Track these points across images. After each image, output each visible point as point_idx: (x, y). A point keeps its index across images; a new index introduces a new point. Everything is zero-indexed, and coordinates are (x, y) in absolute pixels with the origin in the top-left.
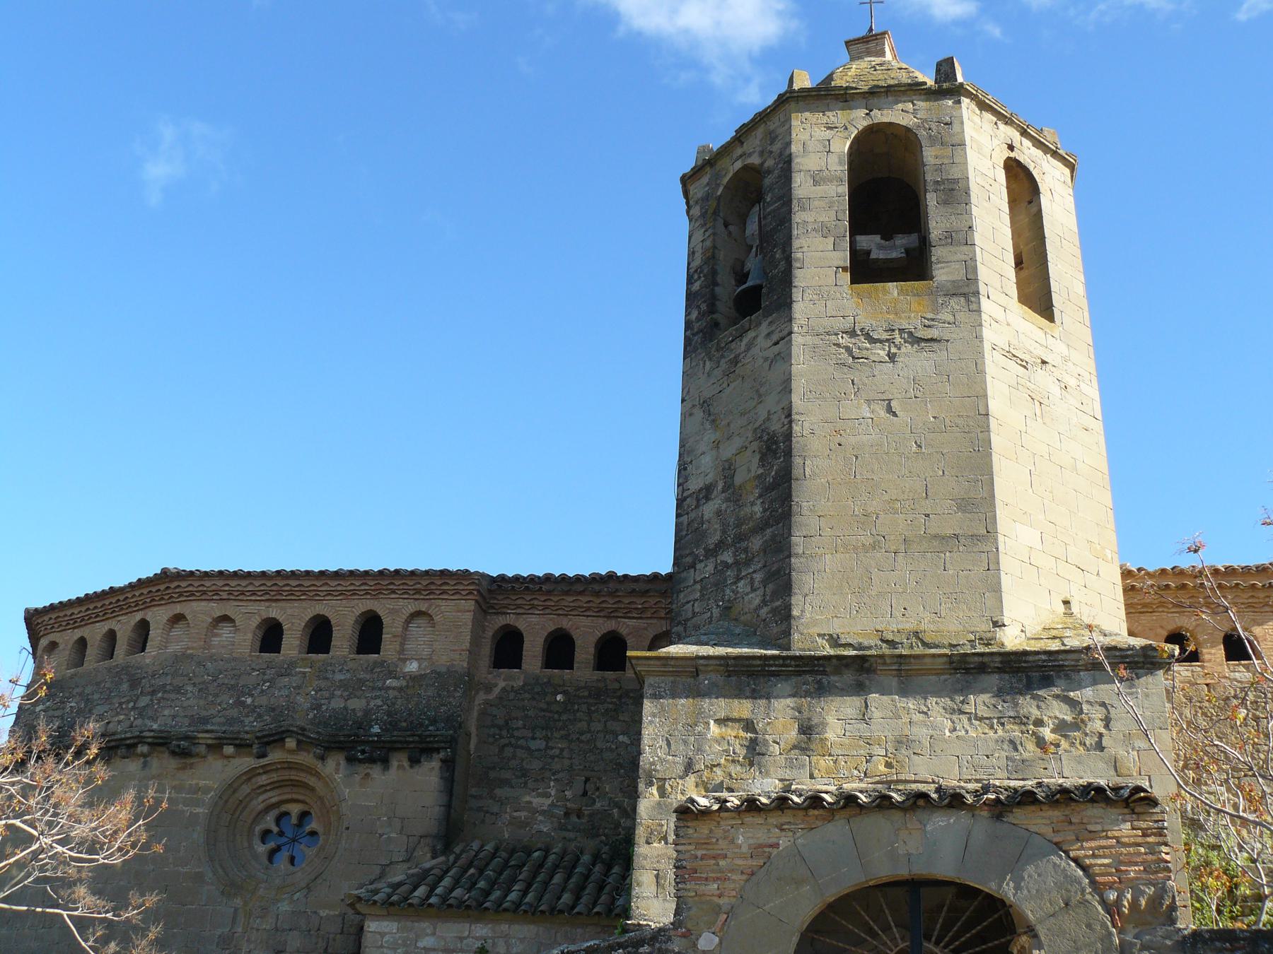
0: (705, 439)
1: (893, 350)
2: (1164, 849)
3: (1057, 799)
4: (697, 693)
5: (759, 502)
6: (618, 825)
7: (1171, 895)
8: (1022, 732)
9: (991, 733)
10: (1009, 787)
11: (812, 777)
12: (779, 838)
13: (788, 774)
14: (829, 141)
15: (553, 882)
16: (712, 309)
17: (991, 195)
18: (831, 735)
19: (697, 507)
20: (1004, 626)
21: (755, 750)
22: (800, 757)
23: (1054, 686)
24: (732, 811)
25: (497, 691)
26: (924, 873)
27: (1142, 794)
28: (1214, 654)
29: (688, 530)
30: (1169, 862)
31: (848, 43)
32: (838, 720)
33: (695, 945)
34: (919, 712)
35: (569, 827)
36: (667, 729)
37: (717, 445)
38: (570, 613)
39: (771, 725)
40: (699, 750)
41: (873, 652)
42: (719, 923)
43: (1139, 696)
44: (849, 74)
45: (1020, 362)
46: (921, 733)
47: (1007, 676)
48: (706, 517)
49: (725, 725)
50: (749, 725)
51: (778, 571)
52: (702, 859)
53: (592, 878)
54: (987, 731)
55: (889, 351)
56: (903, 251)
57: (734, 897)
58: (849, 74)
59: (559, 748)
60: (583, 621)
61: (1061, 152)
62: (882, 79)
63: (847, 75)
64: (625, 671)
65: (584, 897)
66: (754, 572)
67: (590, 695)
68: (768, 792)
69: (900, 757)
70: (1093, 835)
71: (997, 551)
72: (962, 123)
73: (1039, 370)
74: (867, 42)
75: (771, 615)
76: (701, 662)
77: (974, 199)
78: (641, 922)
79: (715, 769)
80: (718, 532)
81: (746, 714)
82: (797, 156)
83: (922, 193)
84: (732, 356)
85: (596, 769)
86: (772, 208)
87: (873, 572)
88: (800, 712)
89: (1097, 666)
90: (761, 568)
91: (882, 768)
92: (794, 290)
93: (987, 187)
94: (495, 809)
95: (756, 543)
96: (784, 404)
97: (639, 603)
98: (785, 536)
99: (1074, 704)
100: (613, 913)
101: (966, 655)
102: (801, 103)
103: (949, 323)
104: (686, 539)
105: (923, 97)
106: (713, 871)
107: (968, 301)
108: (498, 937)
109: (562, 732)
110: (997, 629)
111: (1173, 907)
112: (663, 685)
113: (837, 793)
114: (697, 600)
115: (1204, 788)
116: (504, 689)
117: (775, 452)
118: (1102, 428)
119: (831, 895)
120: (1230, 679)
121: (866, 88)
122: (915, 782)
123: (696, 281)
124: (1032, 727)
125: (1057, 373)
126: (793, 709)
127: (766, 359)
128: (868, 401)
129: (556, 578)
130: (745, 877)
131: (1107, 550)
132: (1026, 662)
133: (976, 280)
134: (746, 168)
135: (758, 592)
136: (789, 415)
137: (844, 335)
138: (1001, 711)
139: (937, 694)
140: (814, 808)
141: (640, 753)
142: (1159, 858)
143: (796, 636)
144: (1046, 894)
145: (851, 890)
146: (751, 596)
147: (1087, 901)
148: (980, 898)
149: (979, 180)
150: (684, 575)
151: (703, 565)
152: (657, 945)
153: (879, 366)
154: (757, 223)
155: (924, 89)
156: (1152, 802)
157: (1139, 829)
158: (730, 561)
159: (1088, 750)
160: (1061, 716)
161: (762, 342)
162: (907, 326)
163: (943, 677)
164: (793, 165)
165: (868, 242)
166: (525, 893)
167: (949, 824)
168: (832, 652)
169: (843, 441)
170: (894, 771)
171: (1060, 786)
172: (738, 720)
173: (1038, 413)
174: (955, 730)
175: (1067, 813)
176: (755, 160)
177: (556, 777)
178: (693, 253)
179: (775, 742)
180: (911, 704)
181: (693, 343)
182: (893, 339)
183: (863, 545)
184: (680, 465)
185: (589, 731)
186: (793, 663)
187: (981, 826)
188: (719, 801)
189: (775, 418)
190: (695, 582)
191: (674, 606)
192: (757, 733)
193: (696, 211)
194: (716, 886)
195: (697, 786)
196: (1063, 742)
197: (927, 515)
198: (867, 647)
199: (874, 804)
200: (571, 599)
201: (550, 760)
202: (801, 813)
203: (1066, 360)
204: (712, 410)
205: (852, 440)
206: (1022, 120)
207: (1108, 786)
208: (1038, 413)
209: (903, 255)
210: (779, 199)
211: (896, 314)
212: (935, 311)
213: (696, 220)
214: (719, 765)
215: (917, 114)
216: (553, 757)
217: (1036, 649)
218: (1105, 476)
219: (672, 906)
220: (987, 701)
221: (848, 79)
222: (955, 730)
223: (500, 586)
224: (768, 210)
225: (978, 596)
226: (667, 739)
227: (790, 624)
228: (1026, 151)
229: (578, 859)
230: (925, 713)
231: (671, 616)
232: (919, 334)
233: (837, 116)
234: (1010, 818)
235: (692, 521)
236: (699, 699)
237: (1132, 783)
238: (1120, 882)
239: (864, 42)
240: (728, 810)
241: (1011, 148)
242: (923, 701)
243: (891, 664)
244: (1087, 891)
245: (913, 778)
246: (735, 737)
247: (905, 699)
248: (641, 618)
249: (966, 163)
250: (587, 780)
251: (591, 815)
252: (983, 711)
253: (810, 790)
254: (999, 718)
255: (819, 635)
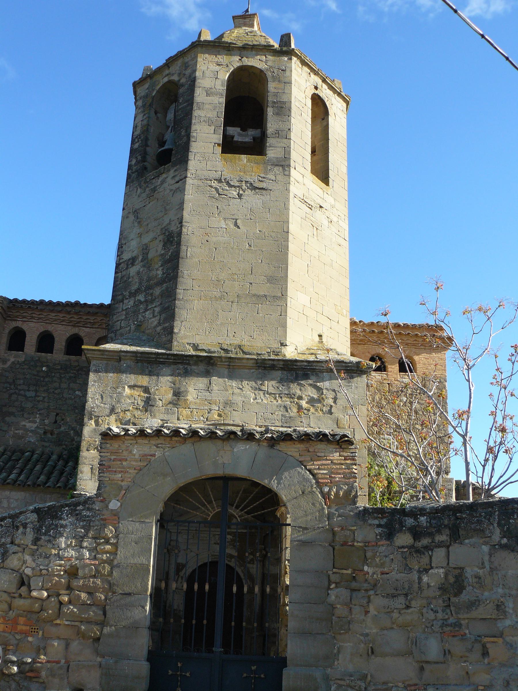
0: (134, 231)
1: (241, 192)
2: (354, 467)
3: (303, 439)
4: (119, 371)
5: (160, 269)
6: (73, 440)
7: (355, 490)
8: (291, 402)
9: (275, 402)
10: (279, 431)
11: (178, 419)
12: (156, 451)
13: (166, 417)
14: (217, 72)
15: (36, 469)
16: (144, 160)
17: (302, 113)
18: (190, 398)
19: (127, 268)
20: (286, 345)
21: (149, 403)
22: (172, 408)
23: (310, 379)
24: (131, 436)
25: (9, 363)
26: (231, 473)
27: (346, 439)
28: (394, 368)
29: (120, 281)
30: (356, 474)
31: (234, 18)
32: (194, 389)
33: (107, 506)
34: (238, 388)
35: (46, 440)
36: (101, 389)
37: (140, 235)
38: (53, 322)
39: (158, 391)
40: (119, 402)
41: (216, 355)
42: (121, 495)
43: (353, 388)
44: (233, 35)
45: (308, 205)
46: (238, 399)
47: (285, 372)
48: (131, 275)
49: (133, 389)
50: (146, 390)
51: (168, 307)
52: (113, 461)
53: (57, 468)
54: (273, 400)
55: (239, 193)
56: (252, 138)
57: (130, 481)
58: (233, 35)
59: (43, 396)
60: (60, 328)
61: (343, 94)
62: (250, 40)
63: (231, 36)
64: (81, 356)
65: (52, 478)
66: (155, 307)
67: (61, 368)
68: (152, 427)
69: (226, 411)
70: (319, 458)
71: (286, 306)
72: (291, 71)
73: (318, 211)
74: (245, 18)
75: (162, 331)
76: (123, 354)
77: (293, 114)
78: (82, 493)
79: (126, 412)
80: (137, 284)
81: (145, 384)
82: (199, 79)
83: (266, 107)
84: (153, 187)
85: (62, 409)
86: (182, 106)
87: (220, 312)
88: (174, 384)
89: (331, 370)
90: (159, 305)
91: (216, 417)
92: (190, 153)
93: (301, 108)
94: (5, 428)
95: (157, 291)
96: (179, 216)
97: (92, 319)
98: (173, 289)
99: (319, 389)
100: (68, 487)
101: (265, 360)
102: (204, 49)
103: (272, 181)
104: (120, 286)
105: (272, 54)
106: (119, 467)
107: (284, 169)
108: (4, 498)
109: (45, 388)
110: (283, 347)
111: (356, 496)
112: (101, 365)
113: (188, 429)
114: (123, 320)
115: (381, 436)
116: (13, 363)
117: (172, 242)
118: (348, 245)
119: (182, 482)
121: (241, 44)
122: (233, 425)
123: (136, 143)
124: (296, 400)
125: (327, 213)
126: (171, 382)
127: (171, 190)
128: (225, 219)
129: (46, 302)
130: (136, 471)
131: (344, 310)
132: (296, 365)
133: (290, 158)
134: (170, 82)
135: (157, 318)
136: (181, 222)
137: (215, 181)
138: (281, 391)
139: (249, 379)
140: (176, 437)
141: (86, 402)
142: (351, 471)
143: (175, 343)
144: (293, 487)
145: (192, 480)
146: (152, 320)
147: (313, 491)
148: (259, 488)
149: (297, 104)
150: (117, 306)
151: (127, 301)
152: (87, 506)
153: (232, 200)
154: (173, 114)
155: (272, 49)
156: (350, 443)
157: (343, 456)
158: (143, 300)
159: (324, 414)
160: (312, 395)
161: (170, 181)
162: (250, 180)
163: (252, 371)
164: (196, 83)
165: (233, 131)
166: (20, 474)
167: (246, 448)
168: (194, 353)
169: (209, 239)
170: (222, 418)
171: (305, 432)
172: (141, 387)
173: (315, 233)
174: (256, 399)
175: (308, 446)
176: (175, 78)
177: (40, 412)
178: (136, 127)
179: (160, 399)
180: (234, 384)
181: (132, 177)
182: (242, 186)
183: (215, 297)
184: (119, 245)
185: (60, 388)
186: (172, 358)
187: (263, 451)
188: (125, 430)
189: (173, 223)
190: (123, 310)
191: (110, 322)
192: (150, 394)
193: (140, 103)
194: (120, 475)
195: (116, 421)
196: (311, 409)
197: (251, 284)
198: (213, 352)
199: (207, 436)
200: (54, 314)
201: (37, 403)
202: (168, 439)
203: (333, 207)
204: (139, 216)
205: (214, 239)
206: (323, 73)
207: (330, 433)
208: (315, 233)
209: (252, 140)
210: (186, 101)
211: (245, 172)
212: (266, 173)
213: (139, 108)
214: (129, 410)
215: (267, 63)
216: (39, 401)
217: (302, 359)
218: (347, 271)
219: (97, 484)
220: (274, 385)
221: (232, 38)
222: (256, 399)
223: (14, 305)
224: (180, 107)
225: (274, 329)
226: (101, 395)
227: (172, 337)
228: (324, 91)
229: (50, 457)
230: (240, 389)
231: (109, 328)
232: (256, 185)
233: (223, 59)
234: (278, 447)
235: (124, 276)
236: (120, 374)
237: (340, 432)
238: (331, 483)
239: (243, 18)
240: (129, 435)
241: (316, 88)
242: (240, 383)
243: (225, 362)
244: (314, 487)
245: (232, 422)
246: (138, 396)
247: (231, 381)
248: (92, 328)
249: (291, 93)
250: (57, 414)
251: (57, 434)
252: (271, 390)
253: (174, 427)
254: (279, 394)
255: (188, 344)
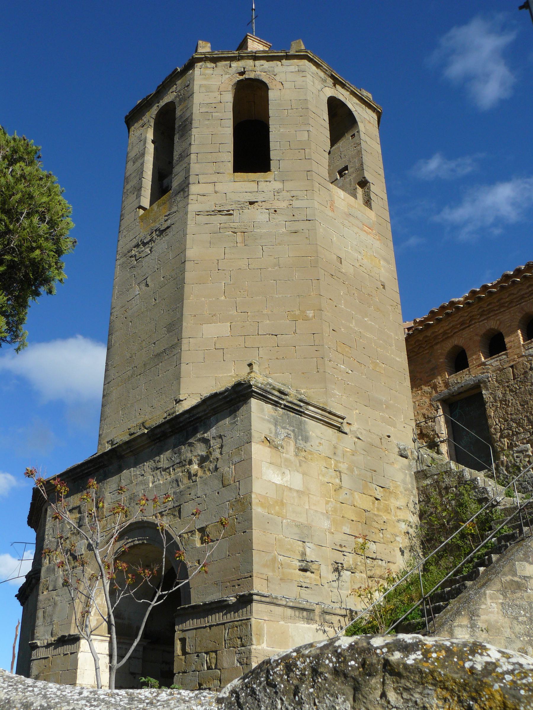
115: (515, 449)
120: (526, 356)
132: (181, 422)
